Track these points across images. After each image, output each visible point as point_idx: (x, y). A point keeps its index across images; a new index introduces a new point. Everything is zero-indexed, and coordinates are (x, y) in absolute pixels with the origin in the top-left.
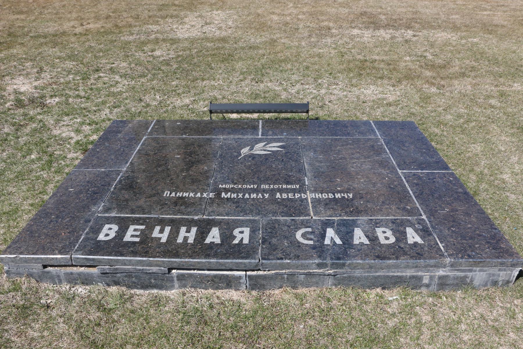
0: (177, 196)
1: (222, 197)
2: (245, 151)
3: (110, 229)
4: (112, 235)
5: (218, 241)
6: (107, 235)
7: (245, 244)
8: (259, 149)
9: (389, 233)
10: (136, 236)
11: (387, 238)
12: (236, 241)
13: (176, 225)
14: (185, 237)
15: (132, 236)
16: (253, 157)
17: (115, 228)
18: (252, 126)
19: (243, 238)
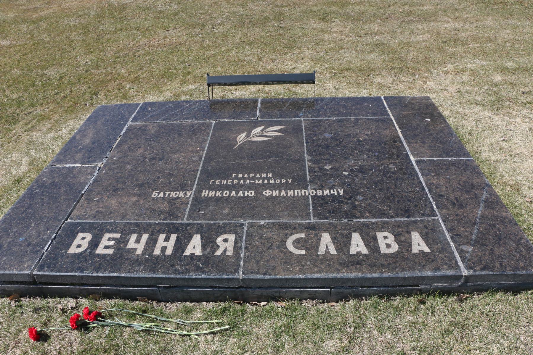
2: (241, 137)
3: (83, 238)
4: (85, 245)
5: (198, 252)
6: (79, 246)
9: (391, 239)
11: (388, 246)
12: (218, 253)
15: (106, 247)
17: (89, 237)
19: (226, 248)
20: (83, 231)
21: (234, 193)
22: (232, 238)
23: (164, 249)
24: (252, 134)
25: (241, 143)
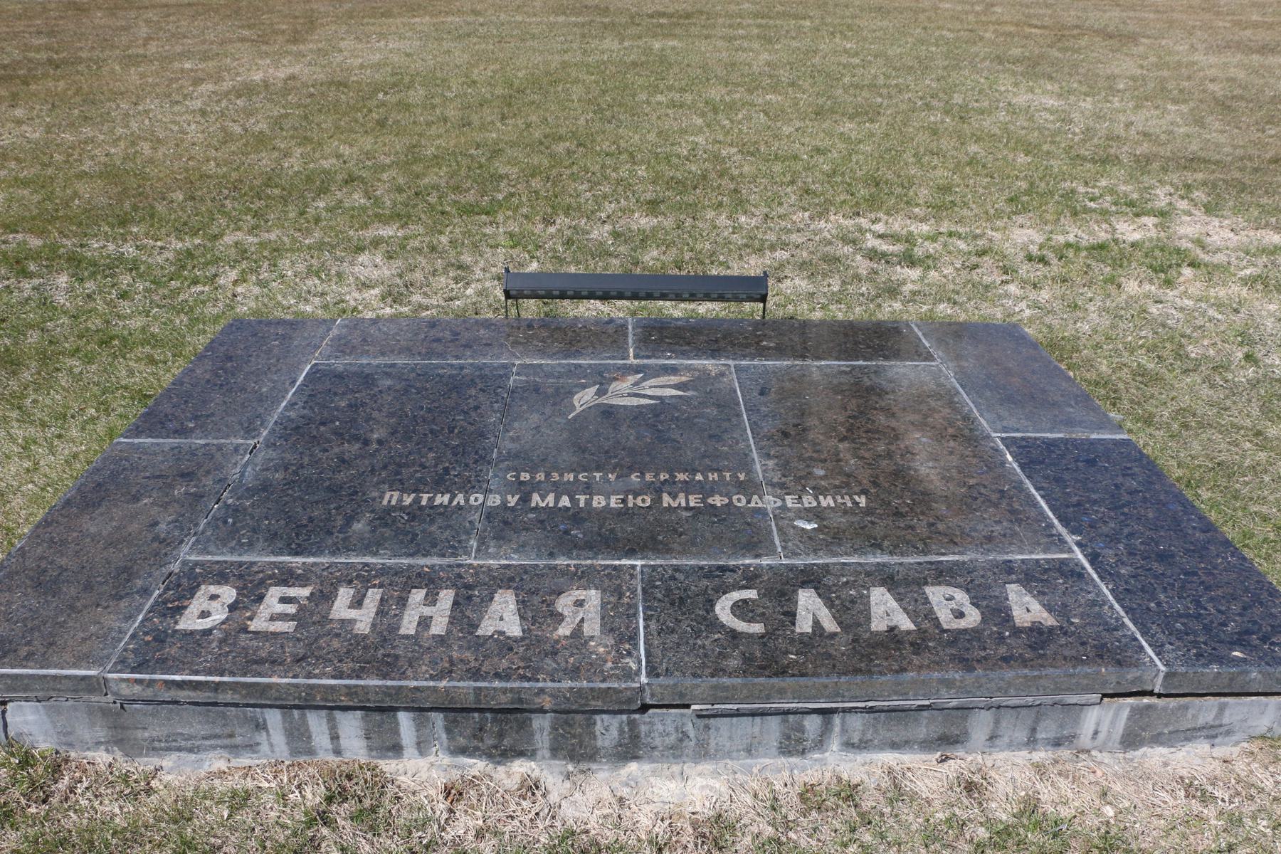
1: (533, 505)
3: (214, 597)
4: (219, 615)
6: (204, 614)
8: (622, 393)
9: (961, 596)
10: (283, 617)
12: (564, 630)
14: (434, 603)
15: (272, 619)
16: (608, 412)
17: (228, 593)
18: (610, 335)
20: (374, 586)
21: (550, 499)
22: (593, 597)
25: (584, 407)
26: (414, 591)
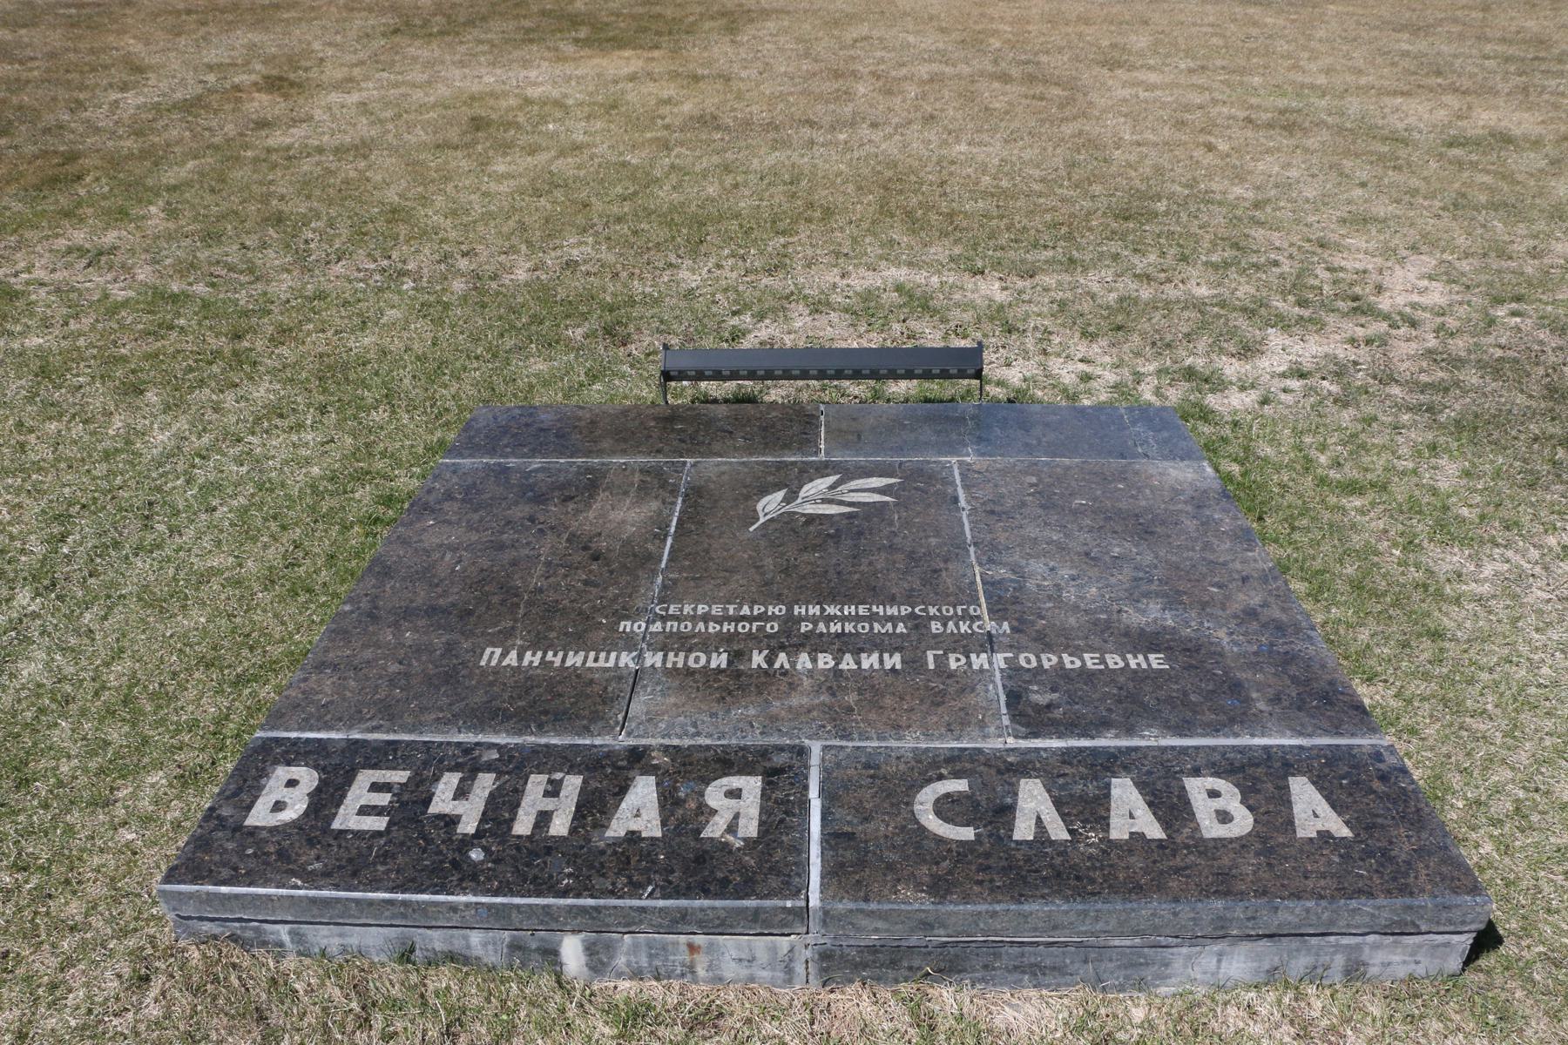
0: (525, 663)
2: (770, 504)
3: (292, 783)
7: (519, 837)
9: (1231, 800)
11: (1224, 817)
13: (514, 767)
15: (365, 811)
17: (308, 778)
22: (752, 785)
23: (544, 818)
24: (802, 494)
26: (480, 775)
